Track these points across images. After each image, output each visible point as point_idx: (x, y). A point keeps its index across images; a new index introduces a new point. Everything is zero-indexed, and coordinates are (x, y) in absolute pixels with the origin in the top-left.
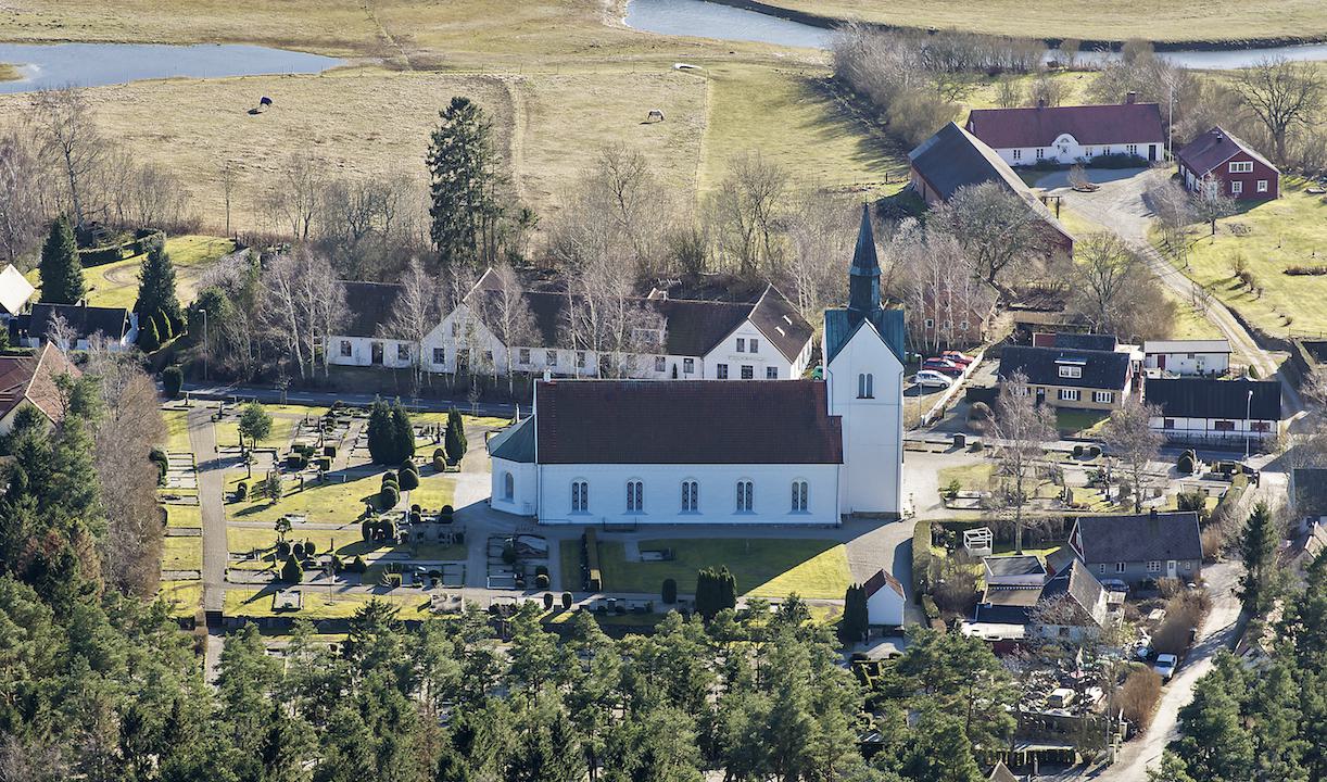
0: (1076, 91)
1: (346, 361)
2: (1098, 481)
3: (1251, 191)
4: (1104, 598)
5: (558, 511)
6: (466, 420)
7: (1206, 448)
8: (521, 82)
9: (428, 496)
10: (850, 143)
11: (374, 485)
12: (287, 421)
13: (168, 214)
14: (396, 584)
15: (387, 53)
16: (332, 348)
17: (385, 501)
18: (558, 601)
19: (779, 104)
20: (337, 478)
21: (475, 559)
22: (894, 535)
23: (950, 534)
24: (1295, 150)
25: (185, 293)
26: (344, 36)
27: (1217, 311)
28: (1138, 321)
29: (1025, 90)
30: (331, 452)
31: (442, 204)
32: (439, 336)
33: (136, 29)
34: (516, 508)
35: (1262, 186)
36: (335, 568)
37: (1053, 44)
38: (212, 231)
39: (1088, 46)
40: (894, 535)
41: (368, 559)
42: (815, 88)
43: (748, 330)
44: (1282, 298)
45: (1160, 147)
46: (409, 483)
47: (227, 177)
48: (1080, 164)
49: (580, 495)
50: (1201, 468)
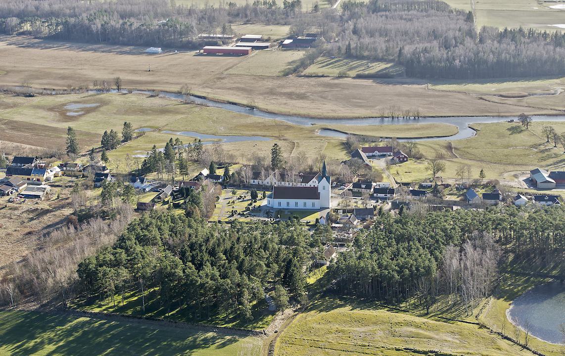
0: (381, 145)
1: (254, 183)
2: (363, 203)
3: (403, 160)
4: (357, 221)
5: (276, 206)
6: (266, 192)
7: (381, 199)
8: (297, 143)
9: (257, 204)
10: (345, 152)
11: (250, 202)
12: (240, 192)
13: (234, 161)
14: (248, 217)
15: (103, 129)
16: (252, 181)
17: (251, 204)
18: (272, 220)
19: (337, 146)
20: (245, 201)
21: (261, 213)
22: (328, 211)
23: (336, 211)
24: (413, 153)
25: (231, 173)
26: (274, 135)
27: (391, 178)
28: (376, 179)
29: (373, 145)
30: (245, 197)
31: (273, 160)
32: (268, 180)
33: (242, 134)
34: (271, 206)
35: (405, 159)
36: (239, 214)
37: (381, 137)
38: (241, 164)
39: (387, 138)
40: (328, 211)
41: (245, 213)
42: (343, 144)
43: (314, 179)
44: (402, 176)
45: (391, 153)
46: (255, 202)
47: (243, 155)
48: (379, 156)
49: (280, 204)
50: (380, 201)
